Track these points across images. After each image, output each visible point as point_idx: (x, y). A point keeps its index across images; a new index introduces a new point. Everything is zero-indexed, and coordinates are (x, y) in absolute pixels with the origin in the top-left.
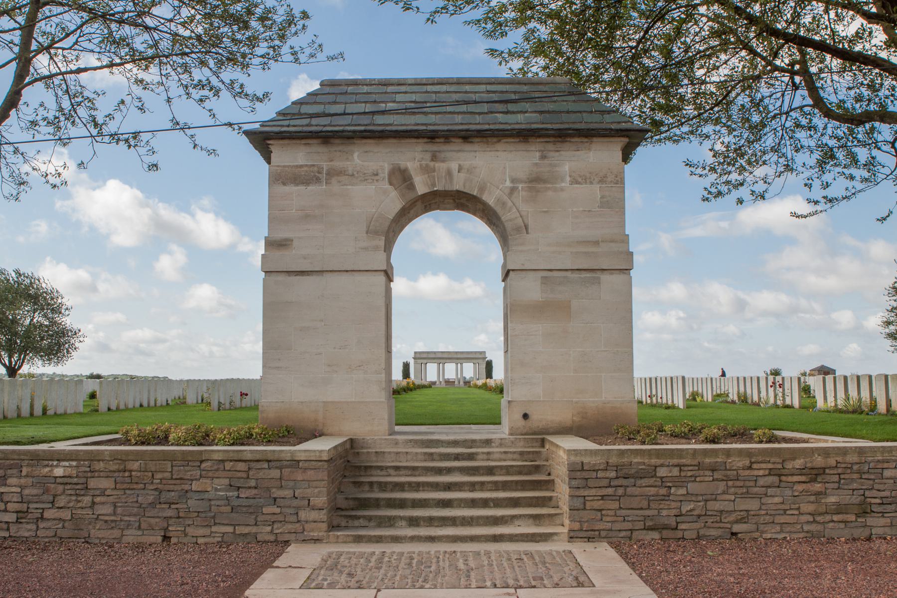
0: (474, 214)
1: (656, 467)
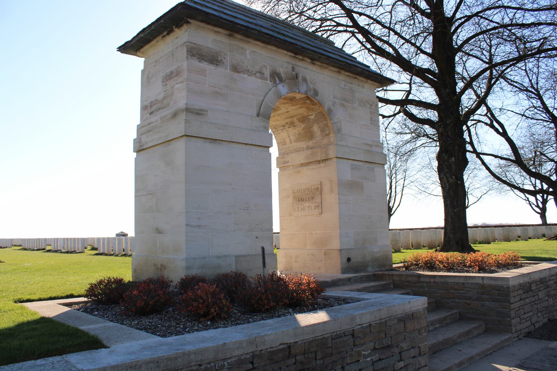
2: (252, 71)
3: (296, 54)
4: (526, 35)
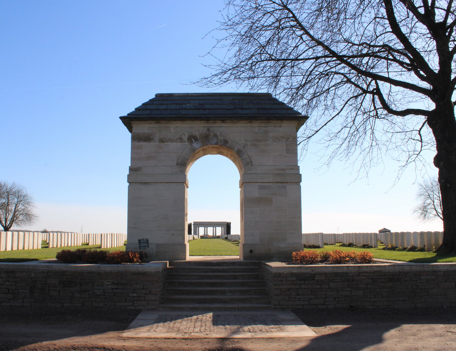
0: (227, 156)
1: (314, 275)
2: (174, 139)
3: (208, 121)
4: (266, 86)
